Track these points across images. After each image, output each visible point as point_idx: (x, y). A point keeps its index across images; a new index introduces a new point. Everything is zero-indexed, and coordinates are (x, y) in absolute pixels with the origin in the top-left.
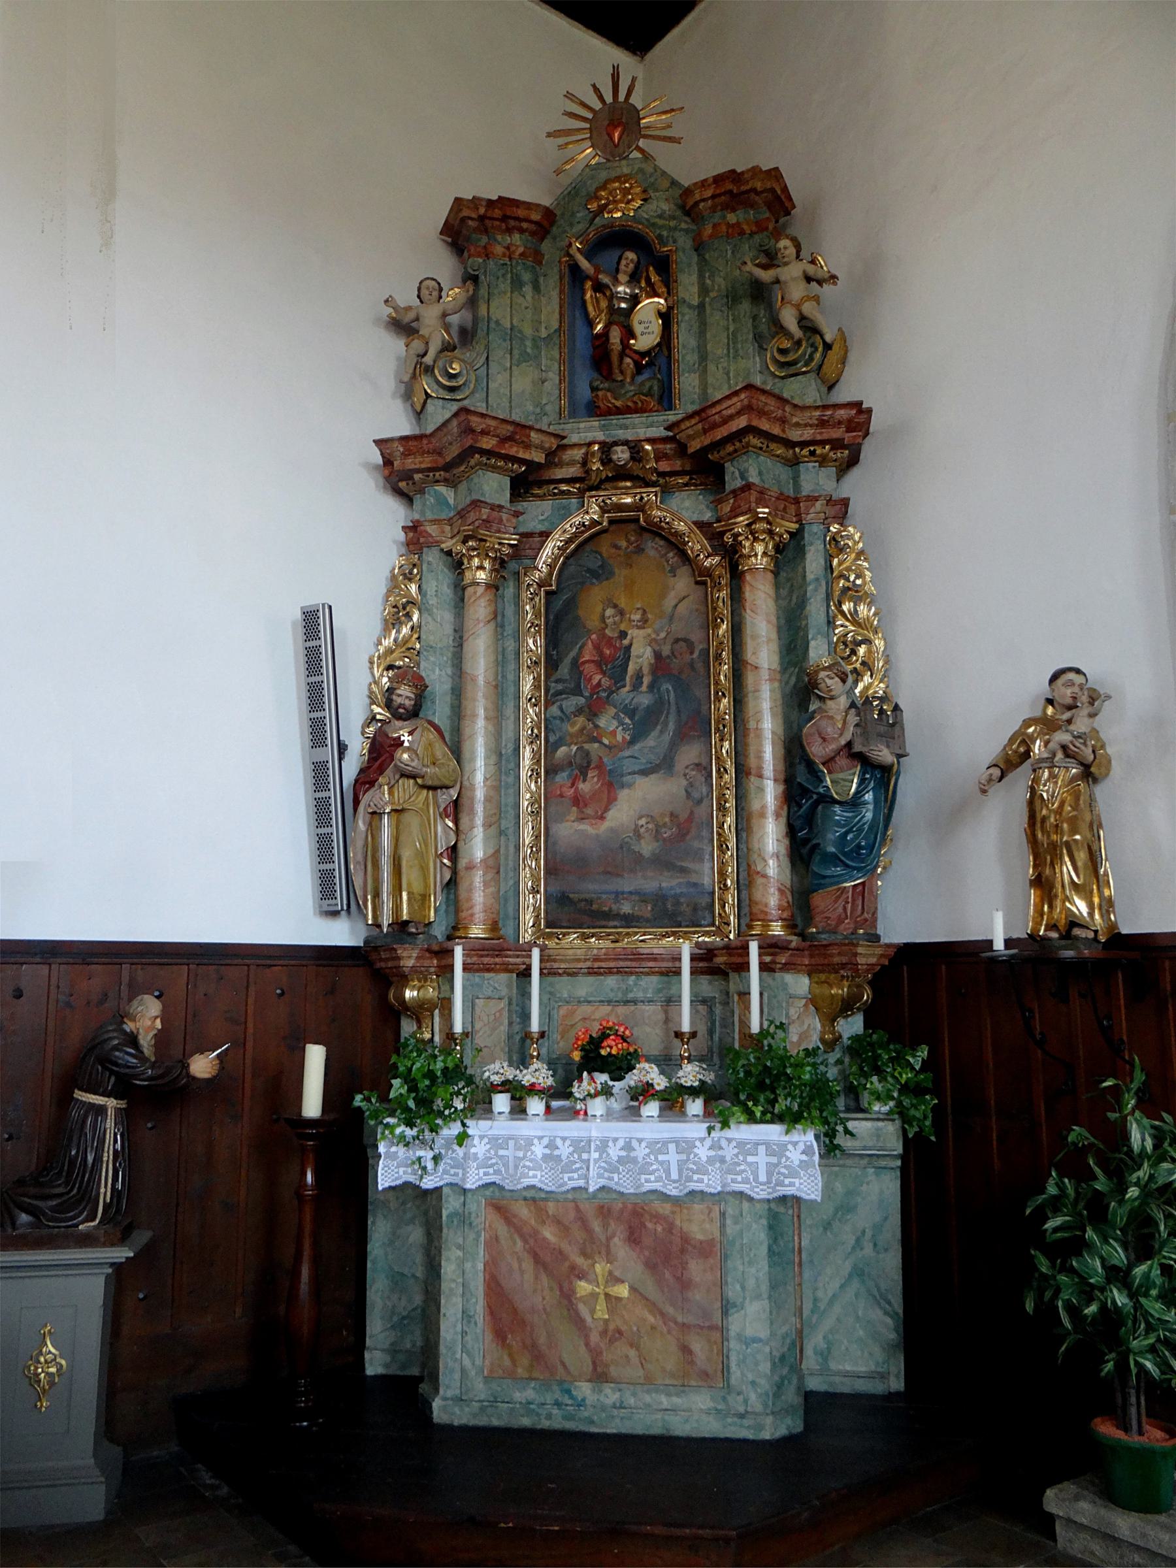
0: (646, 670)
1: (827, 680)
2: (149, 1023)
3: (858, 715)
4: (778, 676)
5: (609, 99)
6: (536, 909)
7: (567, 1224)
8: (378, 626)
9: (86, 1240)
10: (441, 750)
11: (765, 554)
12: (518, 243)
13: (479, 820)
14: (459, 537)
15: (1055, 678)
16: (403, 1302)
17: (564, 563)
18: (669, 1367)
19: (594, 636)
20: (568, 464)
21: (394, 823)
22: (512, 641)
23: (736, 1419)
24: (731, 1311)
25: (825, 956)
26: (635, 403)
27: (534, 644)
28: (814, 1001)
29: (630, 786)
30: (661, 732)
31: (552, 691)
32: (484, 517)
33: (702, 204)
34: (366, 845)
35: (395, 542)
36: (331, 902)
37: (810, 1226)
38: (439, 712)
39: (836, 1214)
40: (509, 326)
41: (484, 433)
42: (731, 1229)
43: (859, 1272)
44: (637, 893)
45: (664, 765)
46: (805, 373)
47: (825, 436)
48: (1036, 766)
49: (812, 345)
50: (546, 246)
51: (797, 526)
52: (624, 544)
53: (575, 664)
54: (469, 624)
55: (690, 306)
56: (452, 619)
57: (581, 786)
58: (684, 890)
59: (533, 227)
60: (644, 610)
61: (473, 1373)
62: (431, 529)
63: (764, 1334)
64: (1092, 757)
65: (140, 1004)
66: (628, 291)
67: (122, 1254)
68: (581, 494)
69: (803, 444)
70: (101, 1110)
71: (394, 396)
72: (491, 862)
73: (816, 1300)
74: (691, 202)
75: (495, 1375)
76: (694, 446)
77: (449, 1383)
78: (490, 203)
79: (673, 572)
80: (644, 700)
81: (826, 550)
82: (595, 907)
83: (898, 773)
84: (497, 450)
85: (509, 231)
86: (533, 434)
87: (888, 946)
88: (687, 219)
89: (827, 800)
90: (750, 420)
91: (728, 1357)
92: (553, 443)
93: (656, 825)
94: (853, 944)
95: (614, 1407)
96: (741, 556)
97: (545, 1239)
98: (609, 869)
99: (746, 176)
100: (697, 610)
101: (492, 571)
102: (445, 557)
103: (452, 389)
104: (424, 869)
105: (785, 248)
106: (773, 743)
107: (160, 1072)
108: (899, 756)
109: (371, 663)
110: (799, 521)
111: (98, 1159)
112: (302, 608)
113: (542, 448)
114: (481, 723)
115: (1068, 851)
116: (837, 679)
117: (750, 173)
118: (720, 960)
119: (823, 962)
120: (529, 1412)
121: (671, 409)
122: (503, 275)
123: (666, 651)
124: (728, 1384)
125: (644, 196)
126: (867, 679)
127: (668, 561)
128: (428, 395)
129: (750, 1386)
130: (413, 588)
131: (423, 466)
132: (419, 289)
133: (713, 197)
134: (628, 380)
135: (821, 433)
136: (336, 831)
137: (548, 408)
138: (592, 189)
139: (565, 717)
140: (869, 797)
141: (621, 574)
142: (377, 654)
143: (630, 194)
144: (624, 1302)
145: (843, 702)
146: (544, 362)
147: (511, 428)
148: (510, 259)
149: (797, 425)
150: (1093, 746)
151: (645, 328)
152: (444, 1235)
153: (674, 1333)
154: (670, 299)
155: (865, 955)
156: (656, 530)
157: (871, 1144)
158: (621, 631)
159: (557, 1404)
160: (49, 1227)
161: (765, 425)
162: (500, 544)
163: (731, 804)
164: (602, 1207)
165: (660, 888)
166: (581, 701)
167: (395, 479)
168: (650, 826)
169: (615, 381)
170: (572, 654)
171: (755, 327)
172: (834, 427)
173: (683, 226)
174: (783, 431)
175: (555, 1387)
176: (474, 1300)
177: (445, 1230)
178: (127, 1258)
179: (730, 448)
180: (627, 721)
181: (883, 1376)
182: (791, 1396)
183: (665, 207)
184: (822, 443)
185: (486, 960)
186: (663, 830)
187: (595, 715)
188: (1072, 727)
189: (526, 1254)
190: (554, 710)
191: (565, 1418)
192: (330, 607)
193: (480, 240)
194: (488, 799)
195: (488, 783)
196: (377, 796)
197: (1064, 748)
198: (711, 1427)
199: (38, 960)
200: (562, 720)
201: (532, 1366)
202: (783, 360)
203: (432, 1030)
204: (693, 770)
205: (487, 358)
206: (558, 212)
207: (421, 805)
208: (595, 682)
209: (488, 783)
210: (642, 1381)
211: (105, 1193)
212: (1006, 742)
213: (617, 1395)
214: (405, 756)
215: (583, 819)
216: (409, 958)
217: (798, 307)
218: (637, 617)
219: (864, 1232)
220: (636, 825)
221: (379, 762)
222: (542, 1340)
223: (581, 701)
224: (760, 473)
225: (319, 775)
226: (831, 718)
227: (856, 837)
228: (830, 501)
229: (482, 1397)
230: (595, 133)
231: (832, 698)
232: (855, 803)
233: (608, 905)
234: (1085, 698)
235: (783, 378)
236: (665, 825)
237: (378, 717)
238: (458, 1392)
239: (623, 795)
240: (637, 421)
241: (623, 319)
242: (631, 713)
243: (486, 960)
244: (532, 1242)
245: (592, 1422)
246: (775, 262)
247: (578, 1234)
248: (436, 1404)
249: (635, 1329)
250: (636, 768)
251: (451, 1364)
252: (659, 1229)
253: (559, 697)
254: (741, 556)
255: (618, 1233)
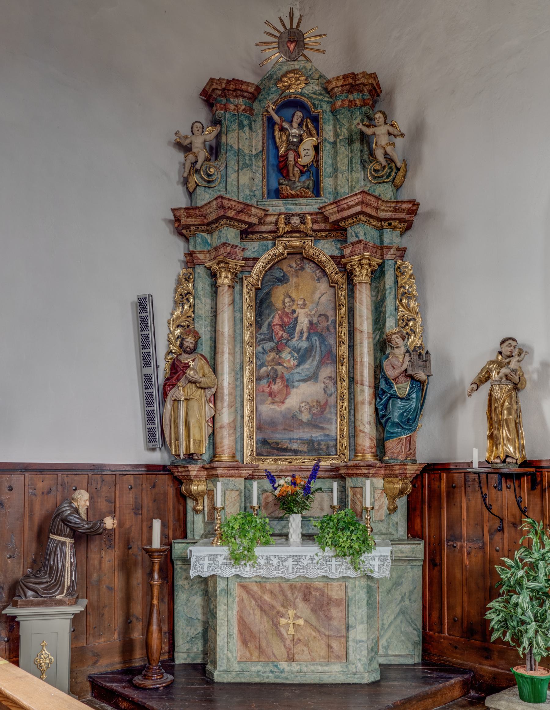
0: (305, 330)
1: (396, 339)
2: (84, 503)
3: (410, 356)
4: (371, 336)
5: (288, 27)
6: (252, 447)
7: (275, 593)
8: (171, 304)
9: (60, 603)
10: (207, 370)
11: (366, 275)
12: (242, 103)
13: (226, 404)
14: (216, 261)
15: (502, 342)
16: (193, 630)
17: (265, 274)
18: (322, 654)
19: (279, 312)
20: (268, 224)
21: (185, 405)
22: (239, 313)
23: (352, 675)
24: (350, 629)
25: (392, 470)
26: (301, 192)
27: (250, 315)
28: (385, 491)
29: (297, 387)
30: (312, 360)
31: (258, 339)
32: (228, 251)
33: (337, 89)
34: (171, 416)
35: (179, 260)
36: (154, 444)
37: (381, 592)
38: (205, 348)
39: (393, 586)
40: (237, 148)
41: (230, 208)
42: (350, 593)
43: (402, 612)
44: (300, 439)
45: (313, 377)
46: (386, 182)
47: (397, 216)
48: (493, 384)
49: (391, 168)
50: (256, 105)
51: (381, 261)
52: (294, 265)
53: (270, 325)
54: (220, 306)
55: (329, 142)
56: (210, 302)
57: (273, 387)
58: (323, 438)
59: (249, 95)
60: (305, 300)
61: (233, 659)
62: (201, 256)
63: (364, 639)
64: (518, 380)
65: (79, 494)
66: (297, 132)
67: (78, 609)
68: (274, 238)
69: (386, 220)
70: (63, 544)
71: (178, 183)
72: (232, 425)
73: (383, 624)
74: (330, 87)
75: (243, 660)
76: (333, 218)
77: (221, 664)
78: (228, 82)
79: (319, 280)
80: (304, 344)
81: (395, 274)
82: (280, 446)
83: (428, 384)
84: (235, 217)
85: (237, 96)
86: (253, 209)
87: (420, 465)
88: (327, 95)
89: (394, 397)
90: (362, 208)
91: (349, 649)
92: (261, 213)
93: (310, 406)
94: (405, 465)
95: (297, 672)
96: (355, 276)
97: (265, 600)
98: (287, 428)
99: (359, 76)
100: (330, 300)
101: (231, 279)
102: (207, 270)
103: (209, 182)
104: (200, 428)
105: (380, 118)
106: (369, 369)
107: (91, 525)
108: (428, 376)
109: (169, 323)
110: (383, 258)
111: (63, 566)
112: (137, 296)
113: (257, 216)
114: (226, 356)
115: (506, 423)
116: (400, 339)
117: (361, 75)
118: (342, 472)
119: (391, 473)
120: (259, 676)
121: (319, 197)
122: (234, 121)
123: (315, 320)
124: (349, 660)
125: (306, 82)
126: (413, 337)
127: (316, 275)
128: (197, 185)
129: (358, 661)
130: (190, 285)
131: (196, 223)
132: (192, 128)
133: (342, 86)
134: (297, 180)
135: (395, 215)
136: (156, 408)
137: (256, 192)
138: (279, 76)
139: (265, 352)
140: (414, 396)
141: (293, 280)
142: (172, 319)
143: (299, 80)
144: (302, 626)
145: (403, 349)
146: (254, 167)
147: (242, 206)
148: (237, 111)
149: (384, 210)
150: (519, 375)
151: (306, 153)
152: (218, 599)
153: (324, 639)
154: (319, 139)
155: (410, 470)
156: (310, 259)
157: (410, 555)
158: (293, 310)
159: (272, 672)
160: (42, 597)
161: (368, 210)
162: (236, 265)
163: (346, 397)
164: (291, 585)
165: (311, 437)
166: (273, 344)
167: (180, 228)
168: (307, 407)
169: (290, 180)
170: (270, 320)
171: (361, 156)
172: (401, 212)
173: (326, 99)
174: (377, 213)
175: (270, 665)
176: (232, 628)
177: (218, 597)
178: (81, 611)
179: (350, 221)
180: (296, 355)
181: (412, 656)
182: (375, 665)
183: (317, 88)
184: (395, 220)
185: (231, 472)
186: (313, 409)
187: (280, 352)
188: (510, 366)
189: (256, 607)
190: (260, 349)
191: (275, 677)
192: (152, 296)
193: (222, 101)
194: (230, 394)
195: (230, 386)
196: (177, 392)
197: (506, 376)
198: (341, 679)
199: (19, 472)
200: (263, 354)
201: (259, 656)
202: (372, 172)
203: (203, 505)
204: (327, 380)
205: (226, 166)
206: (262, 87)
207: (198, 397)
208: (280, 335)
209: (230, 386)
210: (310, 660)
211: (67, 582)
212: (480, 371)
213: (299, 667)
214: (192, 372)
215: (274, 403)
216: (194, 470)
217: (384, 148)
218: (301, 303)
219: (405, 594)
220: (300, 406)
221: (177, 375)
222: (264, 644)
223: (273, 344)
224: (365, 234)
225: (147, 381)
226: (397, 357)
227: (408, 414)
228: (398, 249)
229: (237, 670)
230: (281, 45)
231: (398, 348)
232: (407, 399)
233: (286, 444)
234: (516, 353)
235: (375, 184)
236: (314, 406)
237: (173, 351)
238: (226, 668)
239: (294, 391)
240: (302, 202)
241: (295, 147)
242: (298, 351)
243: (231, 472)
244: (259, 601)
245: (287, 679)
246: (373, 123)
247: (281, 598)
248: (216, 673)
249: (306, 638)
250: (300, 378)
251: (222, 656)
252: (318, 594)
253: (262, 342)
254: (355, 276)
255: (299, 597)
